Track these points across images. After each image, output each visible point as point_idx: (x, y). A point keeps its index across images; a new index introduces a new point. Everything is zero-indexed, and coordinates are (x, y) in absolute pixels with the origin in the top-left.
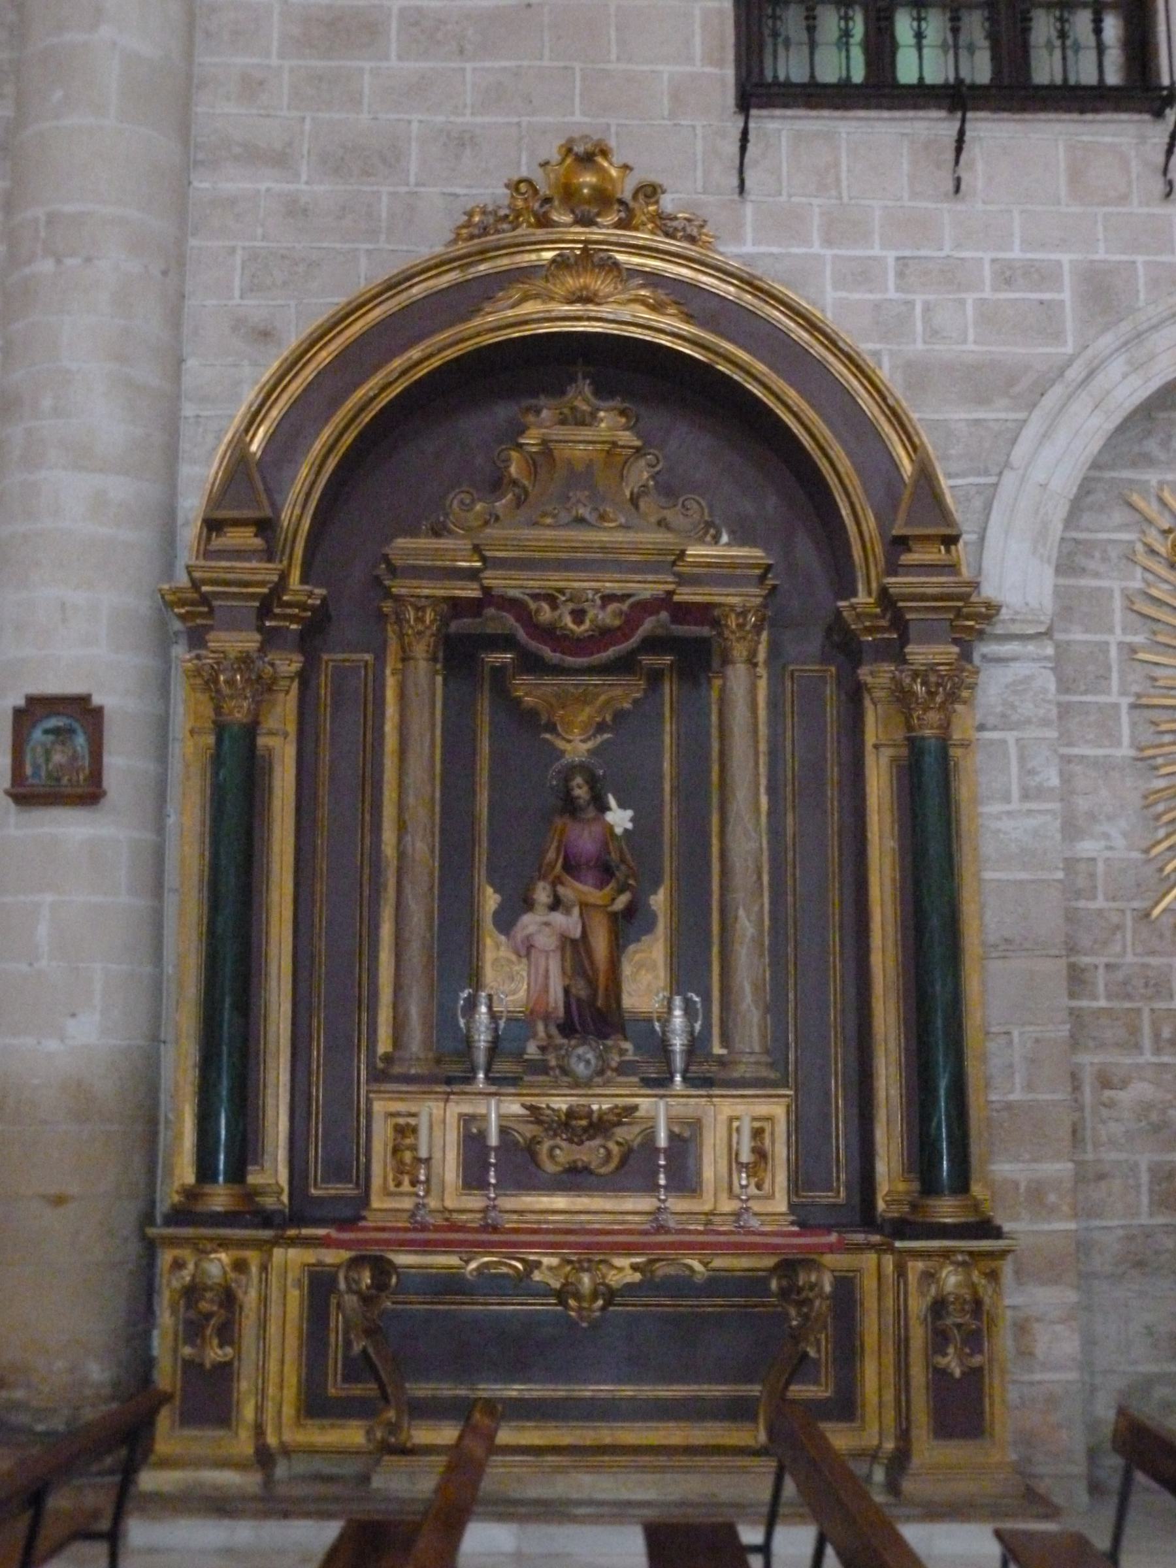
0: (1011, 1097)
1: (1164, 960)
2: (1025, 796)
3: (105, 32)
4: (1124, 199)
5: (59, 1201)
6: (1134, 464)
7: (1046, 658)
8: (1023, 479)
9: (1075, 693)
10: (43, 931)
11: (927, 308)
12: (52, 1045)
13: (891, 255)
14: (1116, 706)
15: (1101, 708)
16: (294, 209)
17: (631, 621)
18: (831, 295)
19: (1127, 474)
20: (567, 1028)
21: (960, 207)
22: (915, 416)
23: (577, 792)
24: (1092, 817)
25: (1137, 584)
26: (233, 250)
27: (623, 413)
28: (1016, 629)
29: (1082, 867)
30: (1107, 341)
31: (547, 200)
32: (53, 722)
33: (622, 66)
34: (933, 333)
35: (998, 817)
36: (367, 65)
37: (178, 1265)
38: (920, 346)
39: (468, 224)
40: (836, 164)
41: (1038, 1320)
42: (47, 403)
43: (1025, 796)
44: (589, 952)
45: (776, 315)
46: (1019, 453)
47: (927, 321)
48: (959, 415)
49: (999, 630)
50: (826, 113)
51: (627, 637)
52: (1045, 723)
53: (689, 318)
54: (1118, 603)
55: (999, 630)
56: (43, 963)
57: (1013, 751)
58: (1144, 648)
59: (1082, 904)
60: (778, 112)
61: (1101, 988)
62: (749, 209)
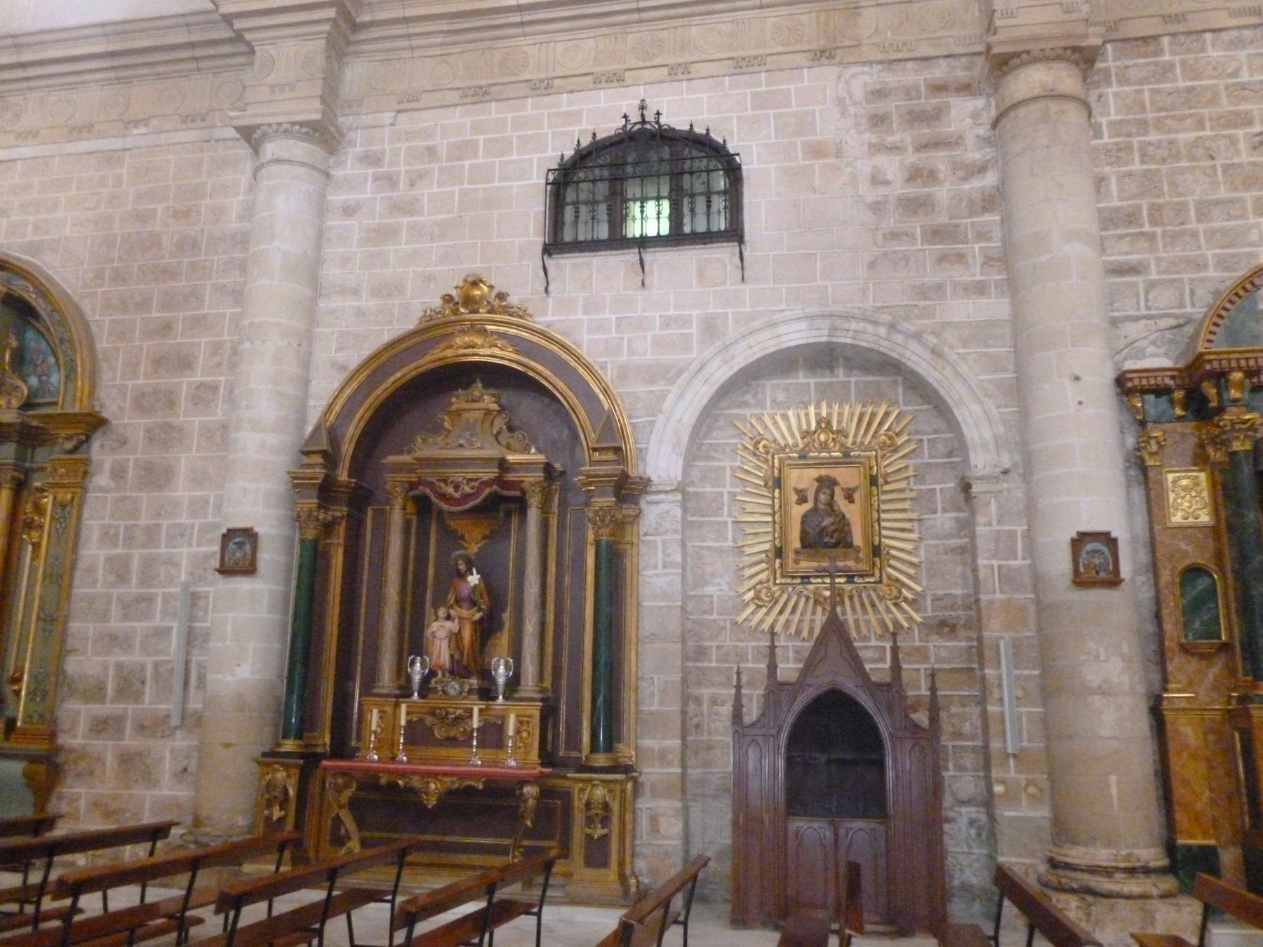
0: (653, 709)
1: (745, 644)
2: (665, 567)
3: (276, 243)
4: (723, 283)
5: (227, 745)
6: (740, 407)
7: (677, 501)
8: (668, 419)
9: (706, 516)
10: (229, 629)
11: (630, 340)
12: (229, 678)
13: (613, 317)
14: (726, 523)
15: (719, 523)
16: (360, 313)
17: (478, 491)
18: (586, 337)
19: (735, 411)
20: (452, 672)
21: (647, 292)
22: (615, 392)
23: (460, 567)
24: (713, 575)
25: (738, 464)
26: (333, 333)
27: (493, 395)
28: (660, 488)
29: (707, 599)
30: (709, 351)
31: (457, 303)
32: (237, 540)
33: (499, 240)
34: (632, 352)
35: (651, 577)
36: (392, 248)
37: (582, 790)
38: (625, 358)
39: (425, 316)
40: (591, 278)
41: (662, 815)
42: (244, 403)
43: (665, 567)
44: (461, 638)
45: (555, 348)
46: (666, 406)
47: (629, 347)
48: (640, 389)
49: (653, 489)
50: (587, 254)
51: (477, 497)
52: (675, 531)
53: (517, 352)
54: (728, 472)
55: (653, 489)
56: (228, 643)
57: (660, 546)
58: (740, 494)
59: (706, 617)
60: (566, 255)
61: (714, 657)
62: (551, 300)
